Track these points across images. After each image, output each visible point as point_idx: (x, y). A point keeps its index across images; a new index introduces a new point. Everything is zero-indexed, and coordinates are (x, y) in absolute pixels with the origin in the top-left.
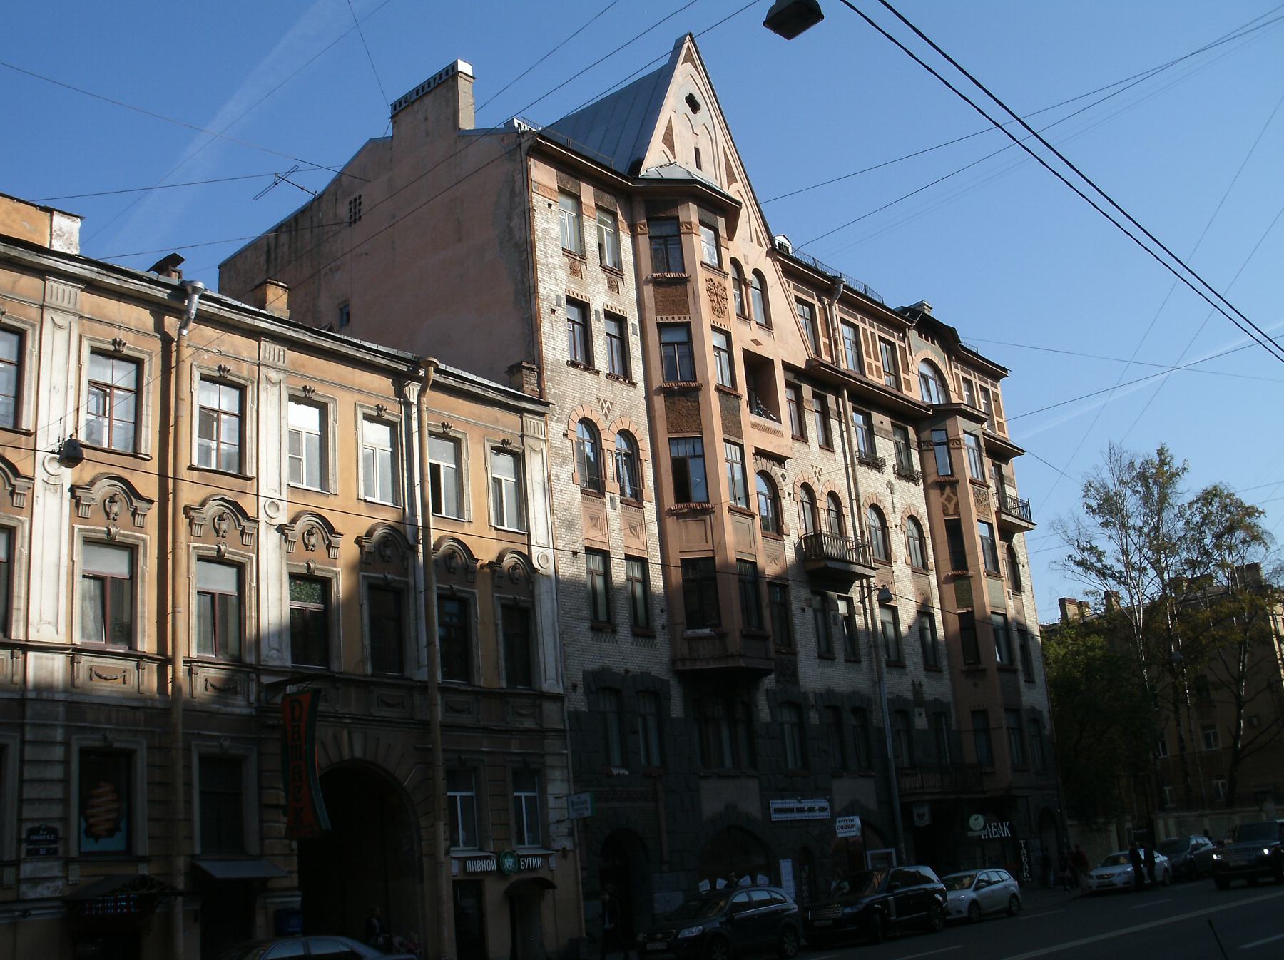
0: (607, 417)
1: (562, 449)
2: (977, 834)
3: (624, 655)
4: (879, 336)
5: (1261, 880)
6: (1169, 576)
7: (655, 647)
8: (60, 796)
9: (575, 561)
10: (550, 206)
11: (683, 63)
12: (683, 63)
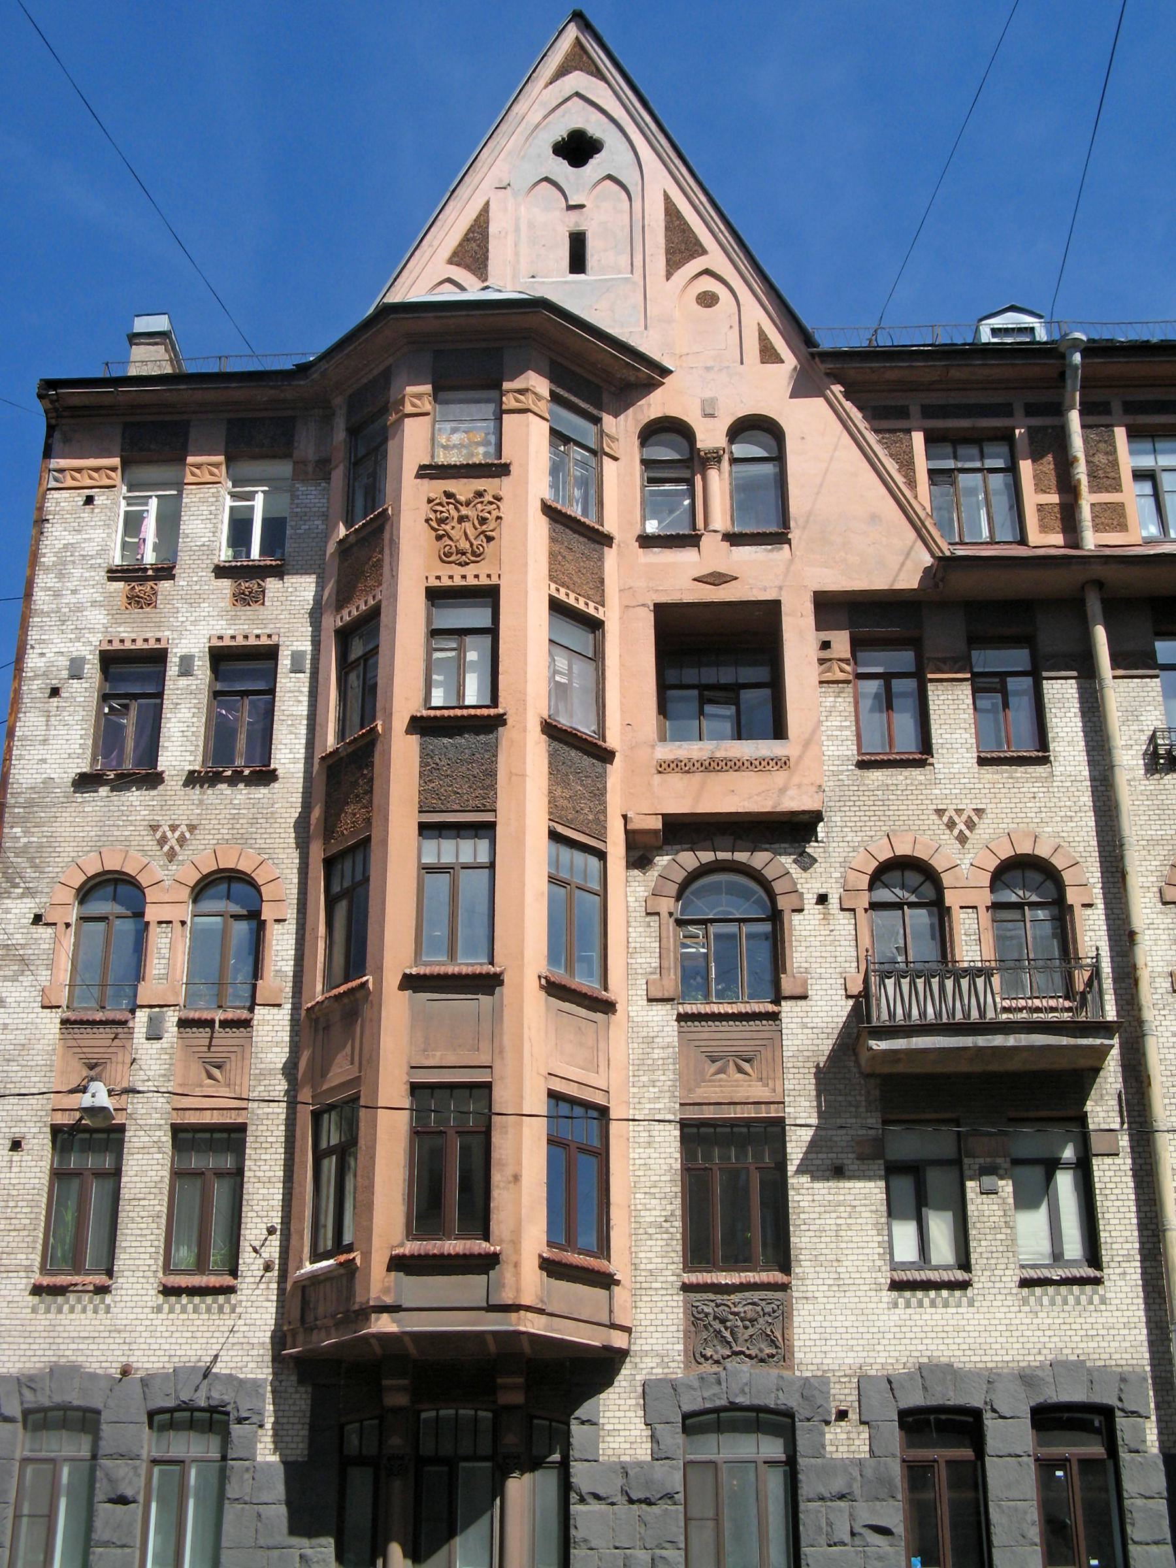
0: (171, 856)
1: (23, 946)
3: (123, 1335)
7: (233, 1311)
9: (15, 1158)
10: (89, 500)
11: (667, 197)
12: (667, 197)
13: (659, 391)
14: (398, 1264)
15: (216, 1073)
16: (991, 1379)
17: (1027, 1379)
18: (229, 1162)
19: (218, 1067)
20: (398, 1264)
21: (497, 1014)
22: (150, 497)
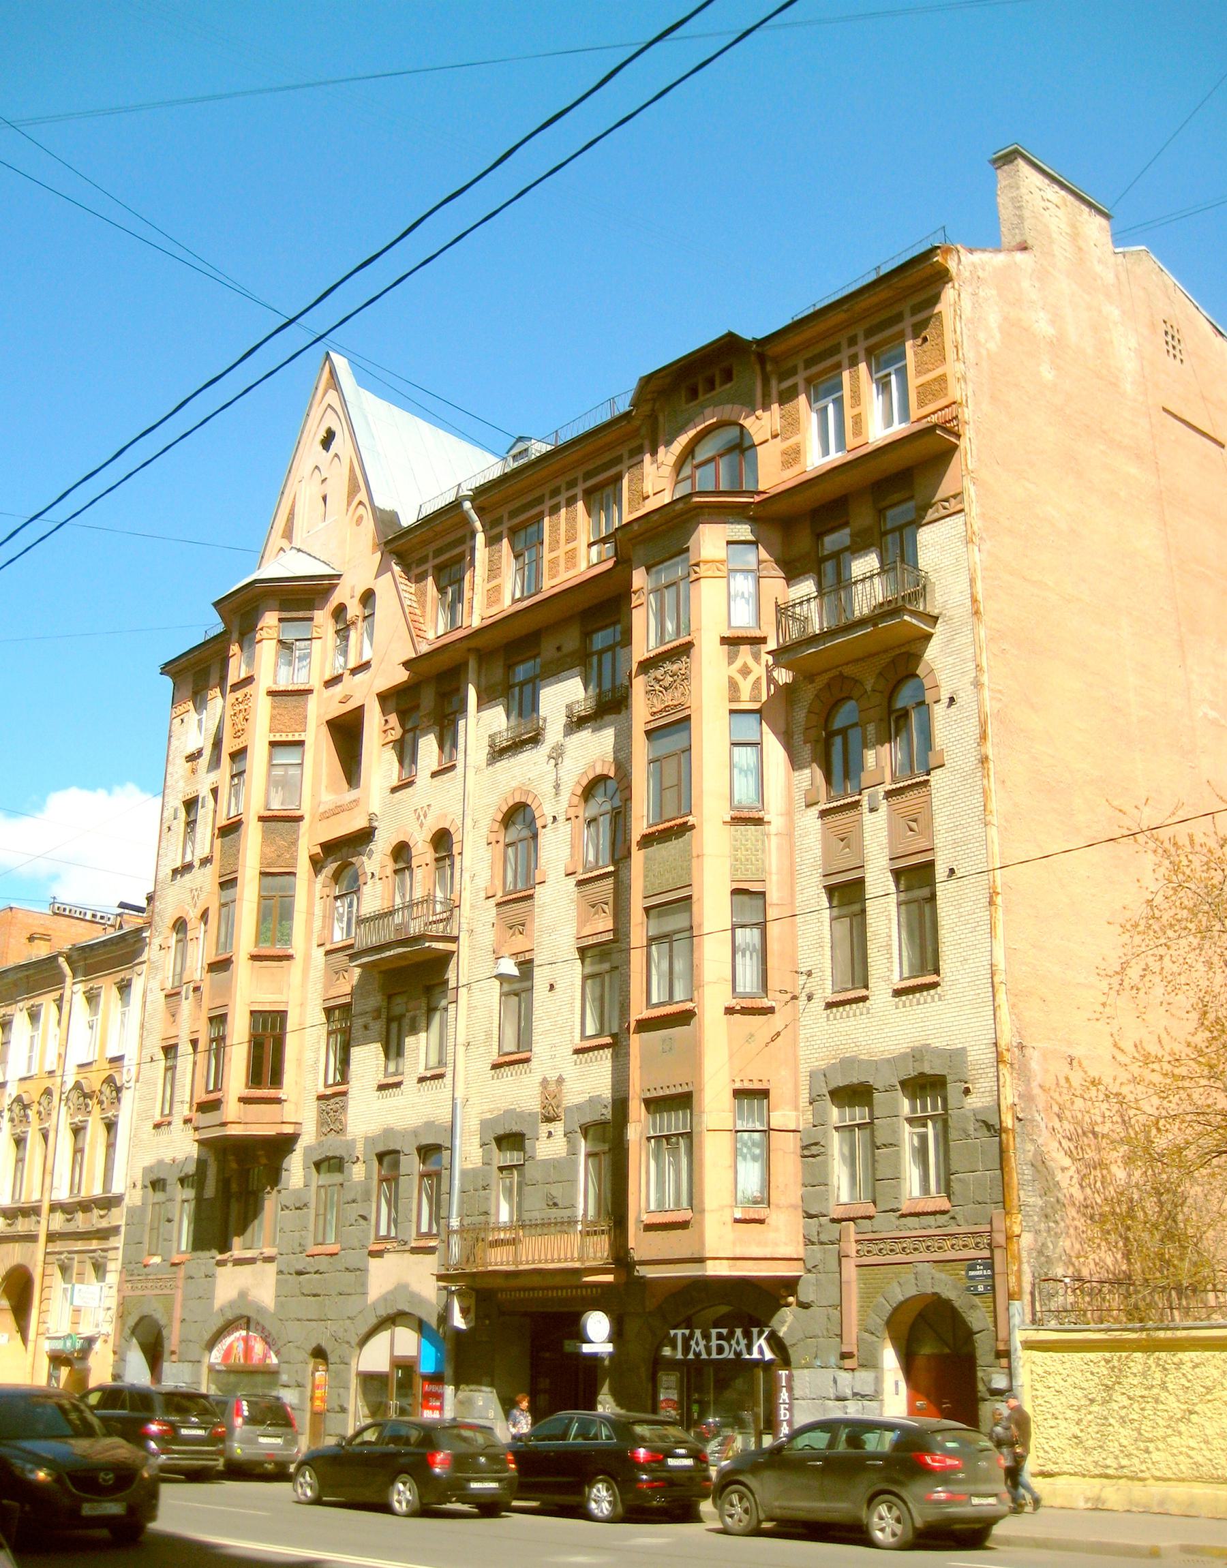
13: (338, 589)
14: (244, 1100)
15: (914, 825)
16: (875, 1065)
17: (416, 1133)
18: (925, 892)
19: (915, 821)
20: (244, 1100)
21: (230, 980)
22: (889, 375)
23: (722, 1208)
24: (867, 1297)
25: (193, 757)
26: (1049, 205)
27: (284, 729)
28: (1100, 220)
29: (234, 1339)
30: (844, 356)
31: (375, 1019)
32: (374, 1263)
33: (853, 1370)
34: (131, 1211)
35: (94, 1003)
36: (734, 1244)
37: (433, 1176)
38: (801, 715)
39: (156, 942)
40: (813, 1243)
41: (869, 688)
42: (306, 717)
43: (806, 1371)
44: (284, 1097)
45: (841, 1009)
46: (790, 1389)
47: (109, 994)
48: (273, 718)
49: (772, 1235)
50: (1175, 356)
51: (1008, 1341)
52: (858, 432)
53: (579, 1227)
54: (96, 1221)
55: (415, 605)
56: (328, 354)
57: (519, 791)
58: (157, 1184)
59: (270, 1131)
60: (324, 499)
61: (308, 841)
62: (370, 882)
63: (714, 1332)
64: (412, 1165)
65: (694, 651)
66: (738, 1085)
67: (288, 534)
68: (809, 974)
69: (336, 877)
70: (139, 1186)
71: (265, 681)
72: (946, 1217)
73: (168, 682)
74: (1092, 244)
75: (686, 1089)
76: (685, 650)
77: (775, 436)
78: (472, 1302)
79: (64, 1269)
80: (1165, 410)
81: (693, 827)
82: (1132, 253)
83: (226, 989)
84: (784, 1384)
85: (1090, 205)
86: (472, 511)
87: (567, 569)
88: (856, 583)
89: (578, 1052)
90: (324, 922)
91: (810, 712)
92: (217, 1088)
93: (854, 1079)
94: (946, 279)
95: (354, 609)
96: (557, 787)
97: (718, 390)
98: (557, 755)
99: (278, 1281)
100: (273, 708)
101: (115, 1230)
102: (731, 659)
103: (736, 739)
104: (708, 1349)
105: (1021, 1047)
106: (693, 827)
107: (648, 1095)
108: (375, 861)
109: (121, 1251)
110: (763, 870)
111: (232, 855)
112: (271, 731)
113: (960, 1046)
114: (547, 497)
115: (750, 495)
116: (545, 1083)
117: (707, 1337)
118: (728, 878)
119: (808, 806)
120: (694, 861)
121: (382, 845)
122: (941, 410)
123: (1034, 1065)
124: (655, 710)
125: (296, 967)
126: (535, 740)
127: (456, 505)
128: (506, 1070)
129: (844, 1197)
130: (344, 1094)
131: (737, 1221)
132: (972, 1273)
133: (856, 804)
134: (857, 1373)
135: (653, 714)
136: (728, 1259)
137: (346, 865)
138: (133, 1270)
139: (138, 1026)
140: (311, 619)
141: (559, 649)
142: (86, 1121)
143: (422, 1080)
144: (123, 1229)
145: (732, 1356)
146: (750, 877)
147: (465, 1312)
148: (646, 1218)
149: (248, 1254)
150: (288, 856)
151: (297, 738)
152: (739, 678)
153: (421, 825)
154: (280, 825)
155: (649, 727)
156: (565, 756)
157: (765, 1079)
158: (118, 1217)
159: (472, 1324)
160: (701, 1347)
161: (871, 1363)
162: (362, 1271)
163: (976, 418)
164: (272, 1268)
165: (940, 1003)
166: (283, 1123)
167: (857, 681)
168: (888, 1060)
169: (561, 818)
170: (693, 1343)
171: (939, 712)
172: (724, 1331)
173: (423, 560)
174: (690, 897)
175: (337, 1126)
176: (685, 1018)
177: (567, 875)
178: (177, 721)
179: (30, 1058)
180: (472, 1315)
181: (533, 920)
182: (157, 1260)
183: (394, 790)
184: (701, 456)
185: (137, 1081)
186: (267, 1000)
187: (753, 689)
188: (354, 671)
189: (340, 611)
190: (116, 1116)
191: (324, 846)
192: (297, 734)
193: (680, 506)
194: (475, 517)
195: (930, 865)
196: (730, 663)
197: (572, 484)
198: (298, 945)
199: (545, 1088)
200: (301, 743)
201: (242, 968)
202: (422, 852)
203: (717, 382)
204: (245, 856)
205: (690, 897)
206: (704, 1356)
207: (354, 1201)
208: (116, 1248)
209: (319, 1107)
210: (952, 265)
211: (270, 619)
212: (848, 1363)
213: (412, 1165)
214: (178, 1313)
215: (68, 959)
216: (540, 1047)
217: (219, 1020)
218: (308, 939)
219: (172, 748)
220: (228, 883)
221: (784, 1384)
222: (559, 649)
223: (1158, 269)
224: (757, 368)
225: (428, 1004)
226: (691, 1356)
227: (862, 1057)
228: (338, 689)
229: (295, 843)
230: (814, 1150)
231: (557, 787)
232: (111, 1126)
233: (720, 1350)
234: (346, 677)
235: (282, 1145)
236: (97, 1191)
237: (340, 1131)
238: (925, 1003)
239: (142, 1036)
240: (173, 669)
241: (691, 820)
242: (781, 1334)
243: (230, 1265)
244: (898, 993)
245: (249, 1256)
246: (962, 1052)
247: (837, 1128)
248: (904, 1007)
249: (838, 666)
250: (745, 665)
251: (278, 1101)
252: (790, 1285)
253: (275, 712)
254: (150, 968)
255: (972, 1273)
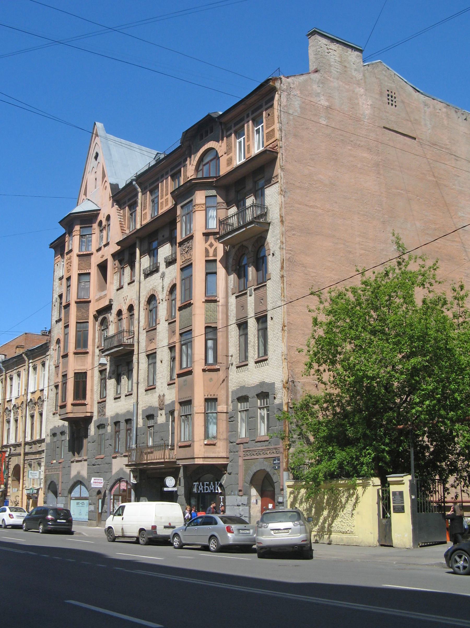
2: (170, 489)
4: (257, 150)
5: (184, 547)
6: (25, 449)
8: (26, 461)
15: (262, 301)
16: (249, 389)
19: (262, 299)
23: (200, 440)
24: (246, 470)
25: (61, 279)
26: (330, 51)
27: (83, 269)
28: (357, 53)
29: (77, 489)
30: (246, 120)
31: (113, 374)
32: (114, 460)
33: (242, 496)
34: (47, 444)
35: (173, 351)
36: (204, 453)
37: (129, 430)
38: (231, 261)
39: (52, 347)
40: (232, 452)
41: (250, 251)
42: (91, 264)
43: (229, 496)
44: (87, 403)
45: (240, 368)
46: (224, 502)
47: (39, 367)
48: (79, 265)
49: (218, 449)
50: (392, 105)
51: (283, 486)
52: (249, 152)
53: (170, 447)
54: (35, 448)
55: (122, 220)
56: (95, 123)
57: (152, 290)
58: (54, 435)
59: (82, 415)
60: (96, 179)
61: (93, 308)
62: (111, 323)
63: (205, 483)
64: (123, 425)
65: (194, 238)
66: (206, 397)
67: (85, 194)
68: (232, 356)
69: (102, 323)
70: (49, 436)
71: (76, 251)
72: (268, 442)
73: (52, 251)
74: (352, 64)
75: (189, 399)
76: (191, 237)
77: (225, 154)
78: (138, 474)
79: (30, 465)
80: (384, 127)
81: (192, 304)
82: (372, 64)
83: (66, 365)
84: (222, 501)
85: (352, 48)
86: (136, 185)
87: (166, 206)
88: (248, 208)
89: (169, 385)
90: (99, 339)
91: (233, 259)
92: (65, 401)
93: (244, 394)
94: (275, 91)
95: (104, 223)
96: (163, 288)
97: (209, 135)
98: (163, 276)
99: (88, 468)
100: (79, 261)
101: (43, 451)
102: (206, 241)
103: (208, 271)
104: (204, 489)
105: (293, 382)
106: (192, 304)
107: (180, 401)
108: (112, 317)
109: (44, 459)
110: (216, 319)
111: (67, 315)
112: (78, 270)
113: (273, 382)
114: (160, 178)
115: (213, 178)
116: (159, 396)
117: (203, 485)
118: (204, 322)
119: (232, 294)
120: (193, 316)
121: (114, 311)
122: (273, 142)
123: (299, 388)
124: (183, 261)
125: (89, 357)
126: (157, 270)
127: (131, 183)
128: (149, 392)
129: (243, 436)
130: (105, 401)
131: (206, 445)
132: (275, 462)
133: (246, 293)
134: (242, 497)
135: (183, 262)
136: (203, 458)
137: (105, 319)
138: (49, 465)
139: (48, 378)
140: (92, 227)
141: (163, 236)
142: (34, 413)
143: (126, 396)
144: (45, 451)
145: (210, 491)
146: (212, 321)
147: (135, 477)
148: (180, 444)
149: (80, 459)
150: (86, 316)
151: (87, 272)
152: (209, 248)
153: (125, 303)
154: (83, 304)
155: (182, 267)
156: (165, 277)
157: (216, 394)
158: (44, 446)
159: (138, 482)
160: (202, 489)
161: (247, 494)
162: (110, 464)
163: (286, 145)
164: (86, 463)
165: (268, 366)
166: (87, 412)
167: (247, 247)
168: (253, 387)
169: (164, 300)
170: (199, 487)
171: (270, 258)
172: (208, 483)
173: (125, 203)
174: (191, 330)
175: (103, 413)
176: (190, 373)
177: (166, 321)
178: (56, 265)
179: (19, 390)
180: (138, 478)
181: (156, 338)
182: (55, 461)
183: (118, 290)
184: (206, 160)
185: (48, 398)
186: (80, 368)
187: (214, 252)
188: (105, 246)
189: (101, 222)
190: (42, 411)
191: (97, 311)
192: (87, 270)
193: (188, 184)
194: (138, 187)
195: (266, 316)
196: (206, 242)
197: (167, 173)
198: (90, 348)
199: (160, 398)
200: (89, 274)
201: (71, 356)
202: (125, 313)
203: (209, 132)
204: (71, 316)
205: (191, 330)
206: (213, 491)
207: (108, 439)
208: (43, 458)
209: (98, 406)
210: (277, 85)
211: (77, 228)
212: (241, 493)
213: (123, 425)
214: (60, 480)
215: (26, 355)
216: (158, 384)
217: (65, 376)
218: (94, 345)
219: (55, 275)
220: (67, 327)
221: (222, 501)
222: (163, 236)
223: (386, 69)
224: (220, 127)
225: (128, 368)
226: (199, 492)
227: (246, 386)
228: (100, 253)
229: (88, 310)
230: (232, 419)
231: (163, 288)
232: (41, 415)
233: (207, 490)
234: (103, 248)
235: (88, 420)
236: (38, 438)
237: (104, 415)
238: (264, 366)
239: (48, 382)
240: (53, 246)
241: (192, 301)
242: (223, 484)
243: (75, 462)
244: (256, 363)
245: (79, 459)
246: (274, 383)
247: (240, 411)
248: (258, 367)
249: (241, 242)
250: (211, 243)
251: (85, 405)
252: (225, 466)
253: (80, 262)
254: (50, 357)
255: (275, 462)
